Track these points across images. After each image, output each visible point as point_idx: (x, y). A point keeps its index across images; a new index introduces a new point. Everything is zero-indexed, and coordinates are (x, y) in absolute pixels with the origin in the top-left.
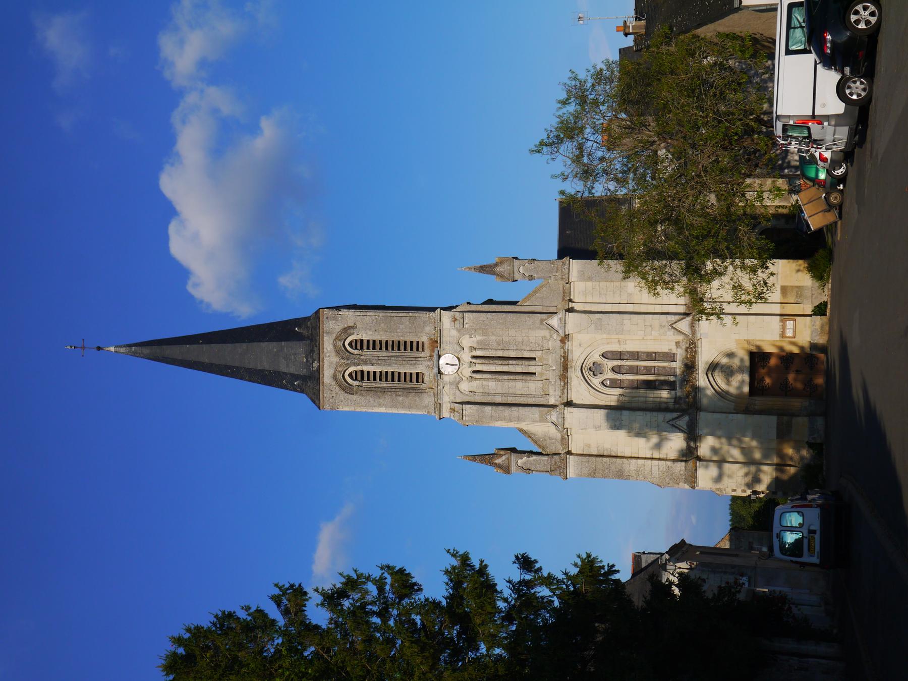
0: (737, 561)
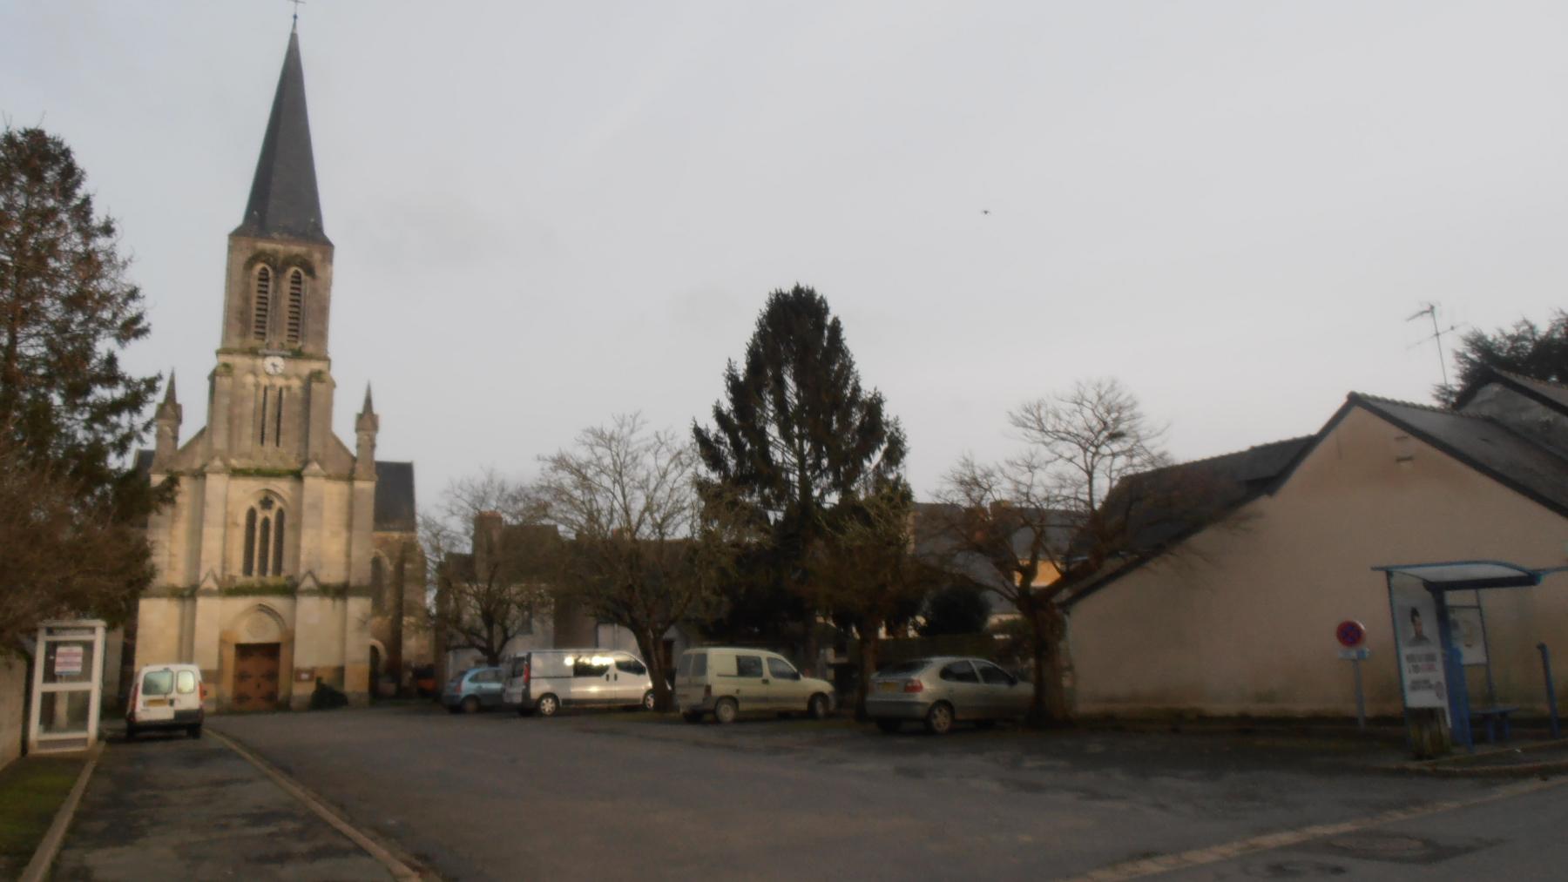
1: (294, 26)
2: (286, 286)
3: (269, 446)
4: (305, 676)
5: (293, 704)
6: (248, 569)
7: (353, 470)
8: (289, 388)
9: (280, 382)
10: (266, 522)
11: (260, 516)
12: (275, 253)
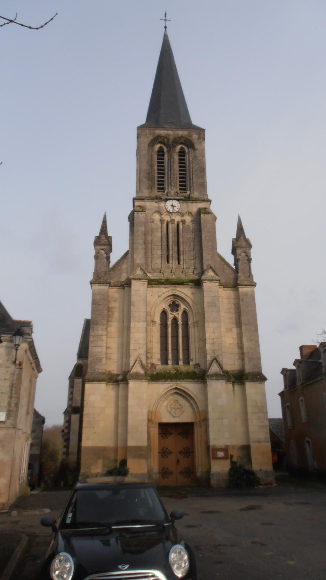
0: (22, 411)
1: (166, 31)
2: (176, 157)
3: (173, 263)
4: (221, 454)
5: (213, 482)
6: (164, 361)
7: (237, 279)
8: (184, 222)
9: (177, 218)
10: (175, 320)
11: (170, 317)
12: (167, 137)
